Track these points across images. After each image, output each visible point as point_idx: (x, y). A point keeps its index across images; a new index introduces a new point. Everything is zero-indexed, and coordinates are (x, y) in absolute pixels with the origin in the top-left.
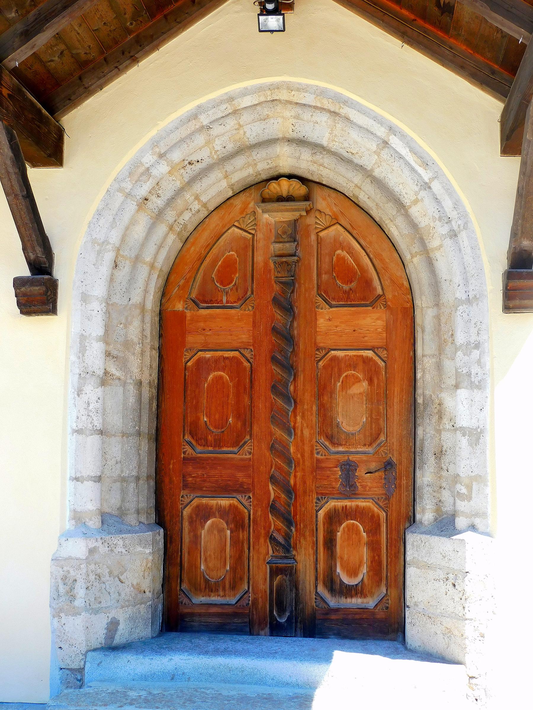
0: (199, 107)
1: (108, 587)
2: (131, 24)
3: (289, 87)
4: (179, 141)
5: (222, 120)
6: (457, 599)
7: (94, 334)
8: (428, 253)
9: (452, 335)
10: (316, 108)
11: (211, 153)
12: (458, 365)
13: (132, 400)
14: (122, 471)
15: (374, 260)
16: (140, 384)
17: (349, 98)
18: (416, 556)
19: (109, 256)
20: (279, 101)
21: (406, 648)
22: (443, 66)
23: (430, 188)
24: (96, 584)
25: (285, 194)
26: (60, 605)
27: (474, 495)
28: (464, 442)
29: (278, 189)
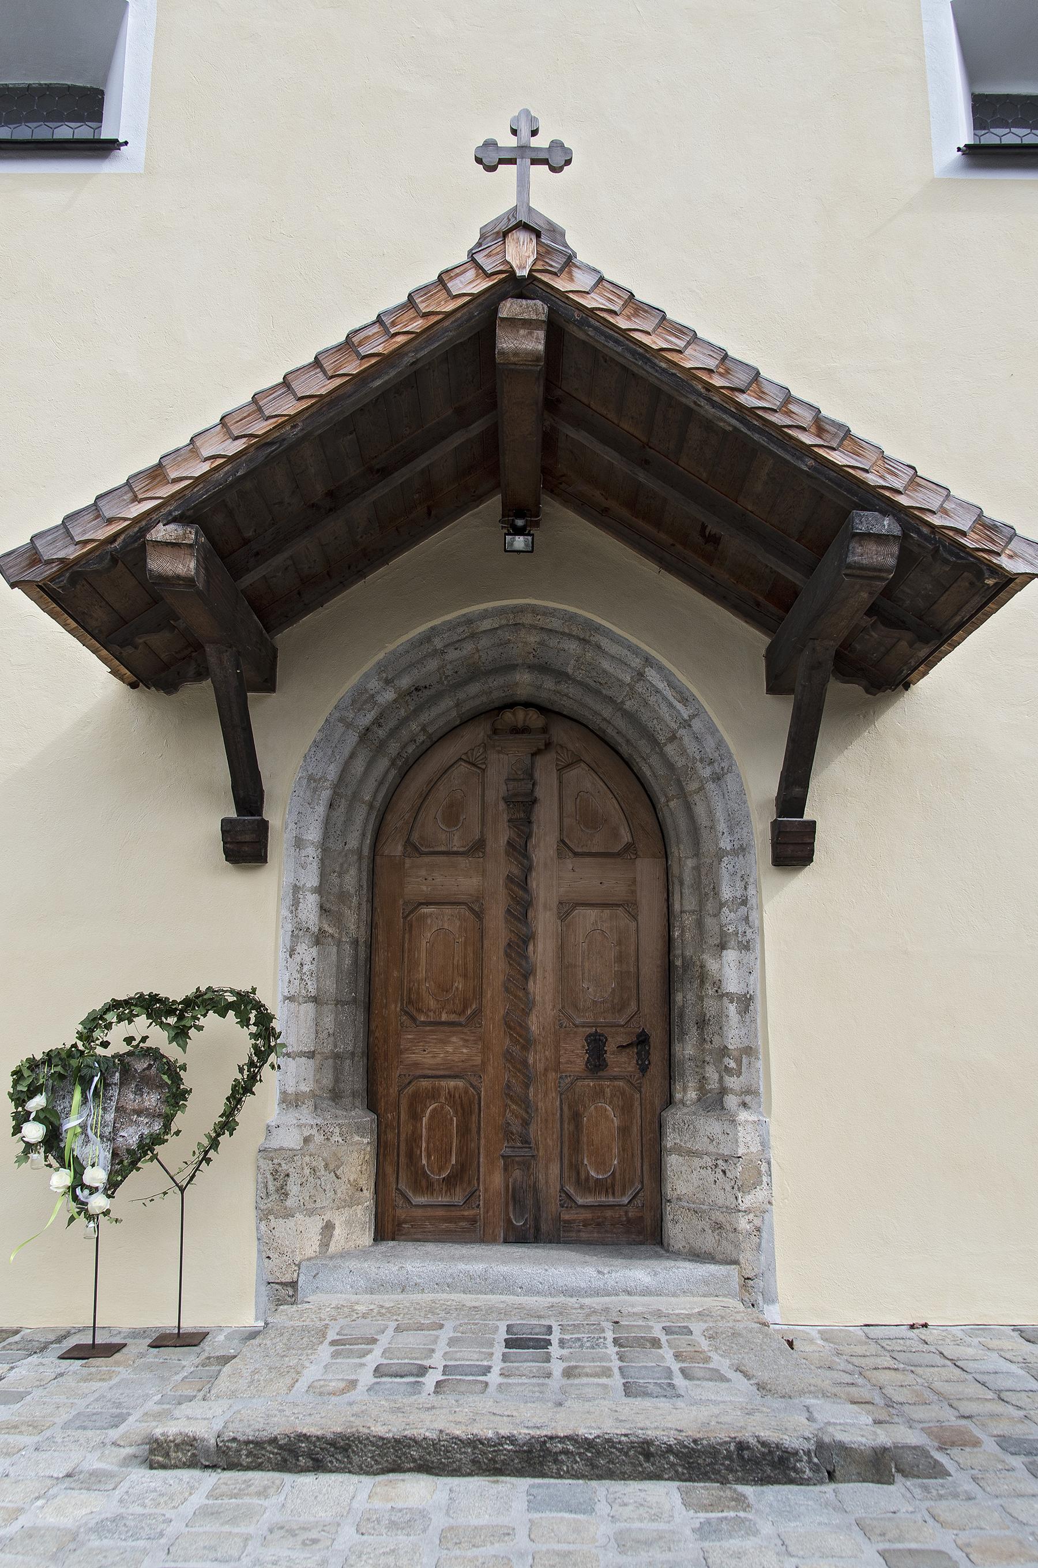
0: (433, 628)
1: (323, 1184)
2: (361, 537)
3: (534, 610)
4: (409, 666)
5: (459, 643)
6: (728, 1188)
7: (308, 885)
8: (686, 797)
9: (714, 888)
10: (563, 634)
11: (441, 678)
12: (724, 923)
13: (348, 961)
14: (336, 1046)
15: (622, 804)
16: (355, 943)
17: (600, 625)
18: (678, 1141)
19: (326, 794)
20: (523, 625)
21: (667, 1251)
22: (704, 594)
23: (690, 726)
24: (311, 1179)
25: (520, 725)
26: (269, 1205)
27: (744, 1069)
28: (732, 1009)
29: (513, 719)
